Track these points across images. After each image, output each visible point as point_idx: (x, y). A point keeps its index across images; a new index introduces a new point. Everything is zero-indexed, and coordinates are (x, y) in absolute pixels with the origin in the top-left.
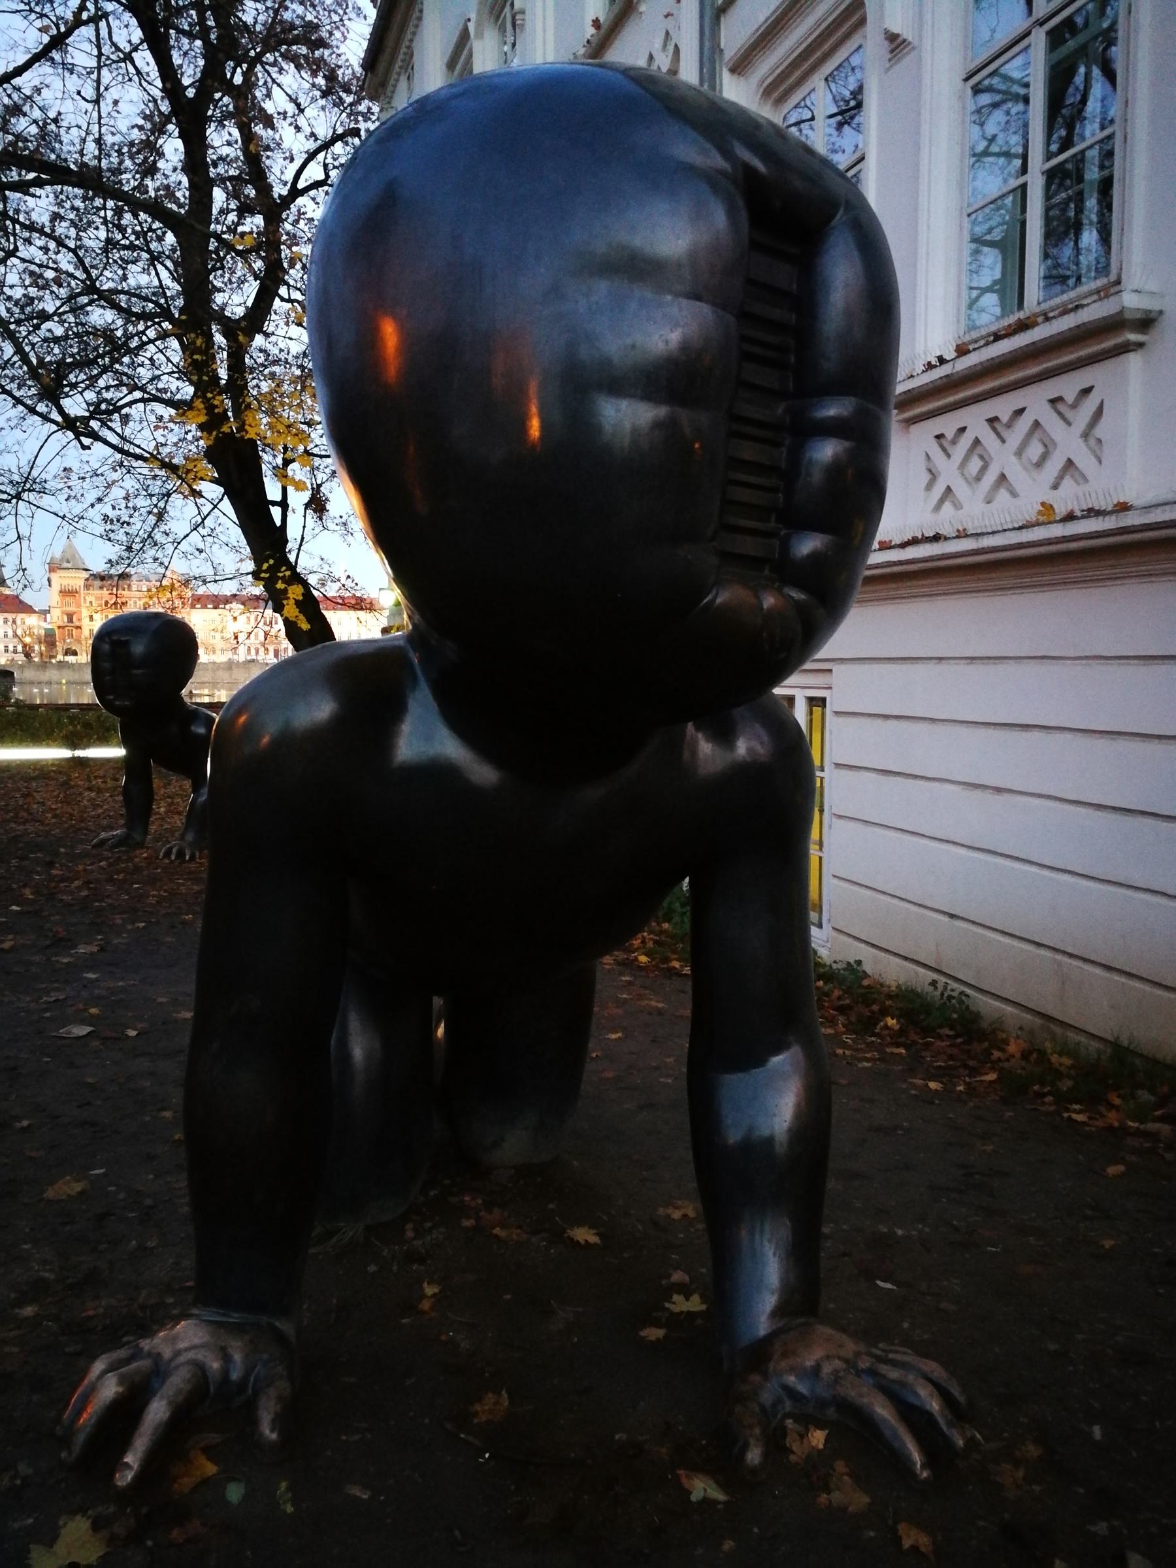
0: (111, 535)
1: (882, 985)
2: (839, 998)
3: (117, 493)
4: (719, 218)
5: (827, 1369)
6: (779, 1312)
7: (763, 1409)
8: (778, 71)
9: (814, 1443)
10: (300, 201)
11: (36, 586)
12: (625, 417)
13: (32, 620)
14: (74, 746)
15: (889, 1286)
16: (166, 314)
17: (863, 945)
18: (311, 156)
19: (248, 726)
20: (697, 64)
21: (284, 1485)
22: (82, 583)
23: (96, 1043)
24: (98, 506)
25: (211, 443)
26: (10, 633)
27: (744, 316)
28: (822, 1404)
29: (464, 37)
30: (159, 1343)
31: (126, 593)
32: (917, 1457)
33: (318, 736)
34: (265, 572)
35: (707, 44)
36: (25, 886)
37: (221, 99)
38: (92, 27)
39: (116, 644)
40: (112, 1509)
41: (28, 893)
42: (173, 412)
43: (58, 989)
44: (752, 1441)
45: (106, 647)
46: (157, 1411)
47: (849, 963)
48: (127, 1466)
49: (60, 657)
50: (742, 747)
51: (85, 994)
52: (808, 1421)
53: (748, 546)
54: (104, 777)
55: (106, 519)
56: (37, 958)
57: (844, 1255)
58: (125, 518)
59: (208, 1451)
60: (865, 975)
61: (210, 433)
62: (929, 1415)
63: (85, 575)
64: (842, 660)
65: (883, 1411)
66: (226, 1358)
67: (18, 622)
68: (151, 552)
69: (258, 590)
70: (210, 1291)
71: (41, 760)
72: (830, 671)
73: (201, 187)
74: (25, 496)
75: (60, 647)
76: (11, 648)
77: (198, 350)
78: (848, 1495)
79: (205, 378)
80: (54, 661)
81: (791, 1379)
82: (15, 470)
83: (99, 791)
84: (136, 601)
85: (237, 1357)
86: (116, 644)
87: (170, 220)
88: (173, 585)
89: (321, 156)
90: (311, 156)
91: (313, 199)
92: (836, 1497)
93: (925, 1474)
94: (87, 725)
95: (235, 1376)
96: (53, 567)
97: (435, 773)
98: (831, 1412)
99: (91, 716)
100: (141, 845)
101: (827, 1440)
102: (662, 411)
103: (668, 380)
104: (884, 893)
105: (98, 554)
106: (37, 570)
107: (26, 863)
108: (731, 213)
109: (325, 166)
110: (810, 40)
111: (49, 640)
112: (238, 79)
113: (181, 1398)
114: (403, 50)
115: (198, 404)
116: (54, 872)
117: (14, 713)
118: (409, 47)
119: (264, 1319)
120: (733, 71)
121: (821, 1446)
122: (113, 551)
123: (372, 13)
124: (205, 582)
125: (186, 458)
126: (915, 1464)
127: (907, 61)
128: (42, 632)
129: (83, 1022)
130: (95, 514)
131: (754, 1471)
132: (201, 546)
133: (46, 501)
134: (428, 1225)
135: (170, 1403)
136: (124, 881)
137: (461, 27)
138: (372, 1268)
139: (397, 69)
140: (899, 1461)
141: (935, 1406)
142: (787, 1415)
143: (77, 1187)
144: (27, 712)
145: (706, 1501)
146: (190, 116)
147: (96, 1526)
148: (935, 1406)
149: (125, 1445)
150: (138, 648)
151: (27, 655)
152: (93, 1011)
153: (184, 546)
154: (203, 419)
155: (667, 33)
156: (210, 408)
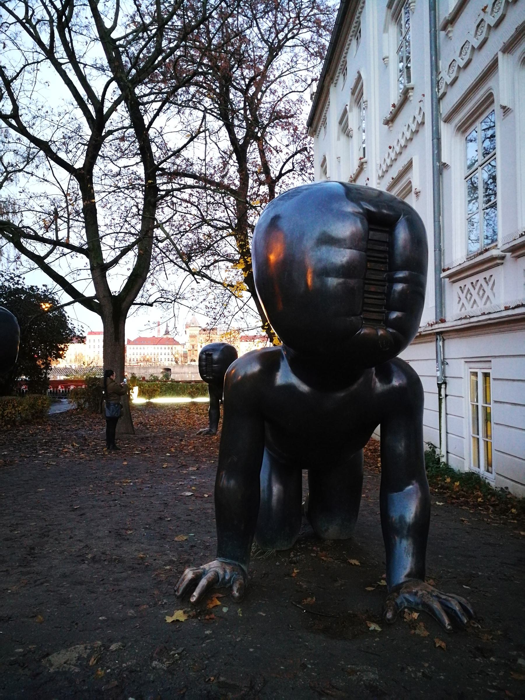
0: (208, 313)
1: (516, 498)
2: (494, 501)
3: (211, 297)
4: (359, 225)
5: (420, 593)
6: (408, 576)
7: (396, 603)
8: (462, 121)
9: (414, 616)
10: (283, 178)
11: (180, 334)
12: (333, 282)
13: (179, 348)
14: (192, 397)
15: (468, 587)
16: (230, 226)
17: (508, 481)
18: (287, 160)
19: (235, 373)
20: (431, 120)
21: (240, 610)
22: (198, 332)
23: (193, 498)
24: (203, 303)
25: (246, 276)
26: (170, 354)
27: (367, 250)
28: (417, 604)
29: (345, 111)
30: (206, 566)
31: (213, 336)
32: (447, 622)
33: (254, 376)
34: (266, 326)
35: (434, 113)
36: (172, 447)
37: (253, 142)
38: (204, 133)
39: (207, 355)
40: (189, 609)
41: (173, 450)
42: (232, 264)
43: (181, 481)
44: (389, 610)
45: (204, 356)
46: (203, 582)
47: (502, 488)
48: (194, 596)
49: (189, 363)
50: (396, 383)
51: (191, 483)
52: (412, 610)
53: (375, 316)
54: (203, 409)
55: (207, 307)
56: (175, 471)
57: (455, 578)
58: (214, 306)
59: (218, 598)
60: (509, 493)
61: (246, 272)
62: (455, 611)
63: (200, 329)
64: (495, 357)
65: (436, 606)
66: (225, 572)
67: (173, 348)
68: (223, 320)
69: (264, 333)
70: (221, 553)
71: (179, 403)
72: (490, 361)
73: (244, 180)
74: (177, 300)
75: (189, 359)
76: (170, 359)
77: (242, 240)
78: (422, 631)
79: (244, 250)
80: (186, 364)
81: (407, 596)
82: (174, 291)
83: (201, 414)
84: (217, 339)
85: (228, 571)
86: (207, 355)
87: (233, 193)
88: (231, 332)
89: (291, 160)
90: (287, 160)
91: (288, 177)
92: (417, 632)
93: (449, 627)
94: (197, 389)
95: (227, 578)
96: (187, 326)
97: (289, 388)
98: (420, 607)
99: (199, 385)
100: (215, 434)
101: (419, 616)
102: (341, 280)
103: (345, 271)
104: (516, 457)
105: (204, 321)
106: (181, 328)
107: (172, 440)
108: (362, 222)
109: (293, 163)
110: (469, 114)
111: (185, 356)
112: (259, 135)
113: (210, 580)
114: (323, 117)
115: (242, 261)
116: (182, 443)
117: (170, 384)
118: (325, 116)
119: (237, 563)
120: (445, 122)
121: (416, 618)
122: (209, 320)
123: (311, 103)
124: (243, 331)
125: (237, 282)
126: (446, 623)
127: (510, 116)
128: (182, 353)
129: (189, 491)
130: (202, 306)
131: (389, 620)
132: (242, 317)
133: (183, 302)
134: (298, 554)
135: (207, 580)
136: (207, 447)
137: (344, 108)
138: (278, 564)
139: (320, 125)
140: (441, 623)
141: (457, 608)
142: (405, 608)
143: (185, 538)
144: (175, 383)
145: (375, 630)
146: (240, 151)
147: (184, 613)
148: (457, 608)
149: (194, 590)
150: (216, 357)
151: (177, 362)
152: (193, 488)
153: (235, 317)
154: (243, 267)
155: (420, 108)
156: (246, 262)
